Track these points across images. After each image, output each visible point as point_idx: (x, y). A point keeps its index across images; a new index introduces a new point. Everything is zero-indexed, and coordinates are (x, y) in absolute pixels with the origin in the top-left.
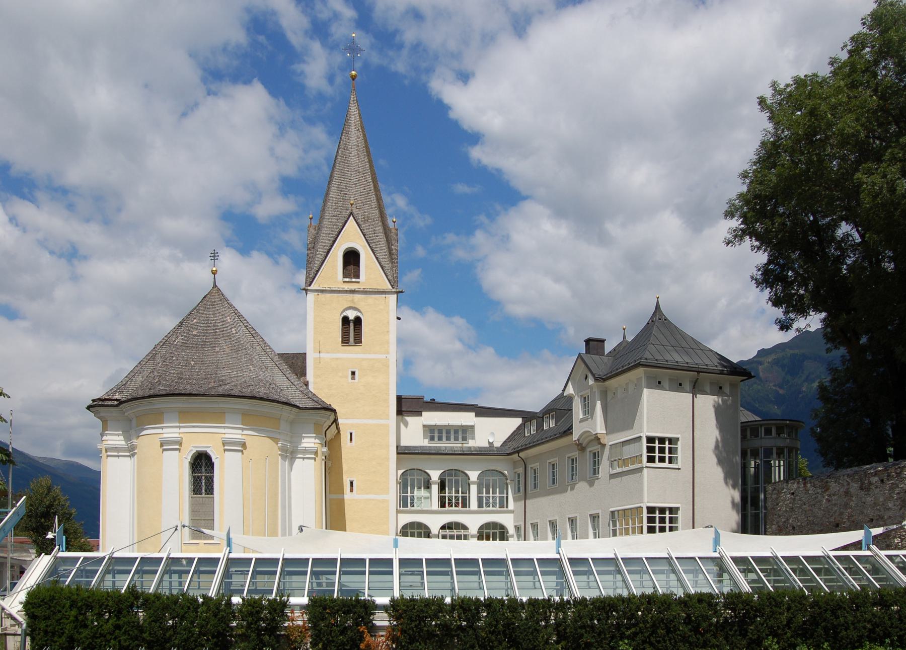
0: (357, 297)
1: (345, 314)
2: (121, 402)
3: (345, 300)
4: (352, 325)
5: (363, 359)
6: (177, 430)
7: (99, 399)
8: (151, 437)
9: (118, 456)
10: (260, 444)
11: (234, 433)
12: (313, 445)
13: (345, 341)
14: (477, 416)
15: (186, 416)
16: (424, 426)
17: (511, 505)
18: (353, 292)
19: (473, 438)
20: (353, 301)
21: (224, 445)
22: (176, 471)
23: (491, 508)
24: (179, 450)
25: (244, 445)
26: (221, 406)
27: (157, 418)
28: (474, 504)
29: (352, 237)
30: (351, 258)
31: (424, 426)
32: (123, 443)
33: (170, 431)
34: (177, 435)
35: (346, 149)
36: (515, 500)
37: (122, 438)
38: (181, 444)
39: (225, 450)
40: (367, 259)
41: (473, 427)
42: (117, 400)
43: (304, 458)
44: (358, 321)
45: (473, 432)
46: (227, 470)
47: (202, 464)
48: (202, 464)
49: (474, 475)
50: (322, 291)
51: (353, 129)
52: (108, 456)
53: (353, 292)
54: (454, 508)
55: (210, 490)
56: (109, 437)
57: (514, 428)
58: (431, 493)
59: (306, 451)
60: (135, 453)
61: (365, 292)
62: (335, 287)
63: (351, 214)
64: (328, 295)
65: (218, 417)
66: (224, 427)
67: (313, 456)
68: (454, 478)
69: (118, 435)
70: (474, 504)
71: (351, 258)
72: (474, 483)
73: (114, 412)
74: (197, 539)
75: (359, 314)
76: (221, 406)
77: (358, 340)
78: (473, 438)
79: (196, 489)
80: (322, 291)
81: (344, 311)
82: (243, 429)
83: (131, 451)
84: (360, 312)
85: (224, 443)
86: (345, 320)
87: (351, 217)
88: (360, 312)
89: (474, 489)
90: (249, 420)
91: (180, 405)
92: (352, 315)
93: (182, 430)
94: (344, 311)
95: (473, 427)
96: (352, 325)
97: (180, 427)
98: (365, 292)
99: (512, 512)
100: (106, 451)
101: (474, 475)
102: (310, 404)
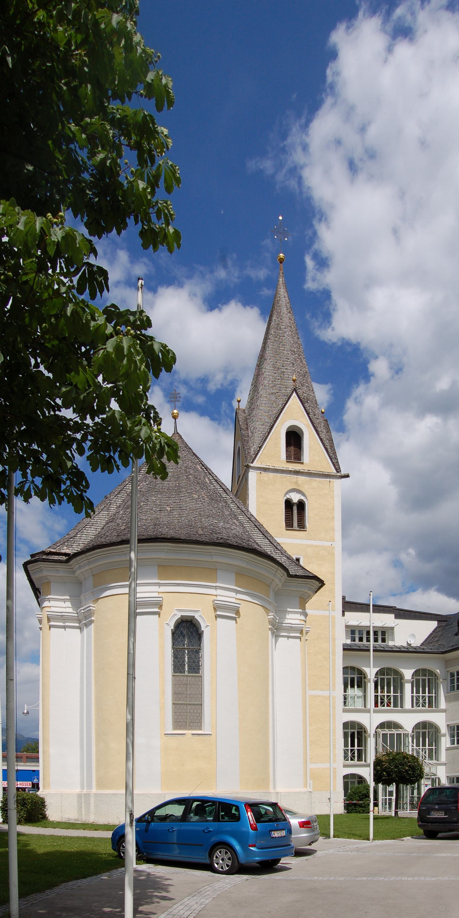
0: (301, 478)
1: (288, 496)
2: (70, 557)
3: (290, 481)
4: (295, 508)
5: (309, 546)
6: (156, 588)
7: (43, 553)
8: (113, 604)
9: (64, 627)
10: (253, 612)
11: (226, 593)
12: (298, 622)
13: (289, 524)
14: (396, 617)
15: (167, 570)
16: (347, 626)
17: (443, 704)
18: (297, 473)
19: (393, 640)
20: (296, 483)
21: (215, 609)
22: (155, 640)
23: (421, 708)
24: (158, 614)
25: (238, 612)
26: (216, 559)
27: (125, 573)
28: (408, 704)
29: (294, 415)
30: (294, 438)
31: (347, 626)
32: (71, 610)
33: (147, 590)
34: (156, 595)
35: (278, 328)
36: (447, 700)
37: (68, 604)
38: (161, 607)
39: (217, 616)
40: (310, 440)
41: (392, 629)
42: (65, 554)
43: (288, 637)
44: (301, 505)
45: (393, 633)
46: (220, 643)
47: (187, 631)
48: (187, 631)
49: (408, 674)
50: (265, 470)
51: (284, 310)
52: (50, 627)
53: (297, 473)
54: (386, 708)
55: (196, 667)
56: (52, 603)
57: (431, 631)
58: (365, 692)
59: (291, 629)
60: (92, 622)
61: (309, 474)
62: (278, 466)
63: (295, 390)
64: (271, 475)
65: (209, 572)
66: (216, 588)
67: (298, 635)
68: (386, 677)
69: (64, 601)
70: (408, 704)
71: (294, 438)
72: (408, 681)
73: (60, 571)
74: (180, 729)
75: (302, 498)
76: (216, 559)
77: (302, 526)
78: (393, 640)
79: (178, 667)
80: (265, 470)
81: (287, 493)
82: (237, 592)
83: (84, 620)
84: (303, 494)
85: (216, 608)
86: (289, 504)
87: (294, 394)
88: (303, 494)
89: (408, 687)
90: (245, 580)
91: (163, 556)
92: (295, 498)
93: (163, 589)
94: (287, 493)
95: (392, 629)
96: (295, 508)
97: (159, 585)
98: (309, 474)
99: (444, 711)
100: (49, 620)
101: (408, 674)
102: (300, 573)
